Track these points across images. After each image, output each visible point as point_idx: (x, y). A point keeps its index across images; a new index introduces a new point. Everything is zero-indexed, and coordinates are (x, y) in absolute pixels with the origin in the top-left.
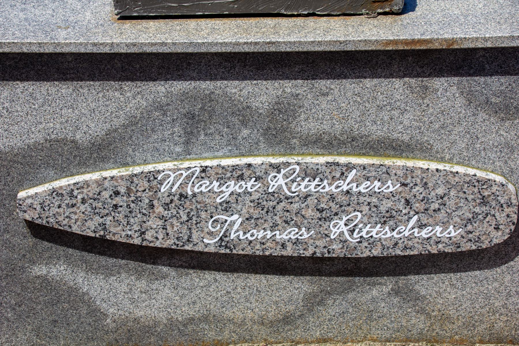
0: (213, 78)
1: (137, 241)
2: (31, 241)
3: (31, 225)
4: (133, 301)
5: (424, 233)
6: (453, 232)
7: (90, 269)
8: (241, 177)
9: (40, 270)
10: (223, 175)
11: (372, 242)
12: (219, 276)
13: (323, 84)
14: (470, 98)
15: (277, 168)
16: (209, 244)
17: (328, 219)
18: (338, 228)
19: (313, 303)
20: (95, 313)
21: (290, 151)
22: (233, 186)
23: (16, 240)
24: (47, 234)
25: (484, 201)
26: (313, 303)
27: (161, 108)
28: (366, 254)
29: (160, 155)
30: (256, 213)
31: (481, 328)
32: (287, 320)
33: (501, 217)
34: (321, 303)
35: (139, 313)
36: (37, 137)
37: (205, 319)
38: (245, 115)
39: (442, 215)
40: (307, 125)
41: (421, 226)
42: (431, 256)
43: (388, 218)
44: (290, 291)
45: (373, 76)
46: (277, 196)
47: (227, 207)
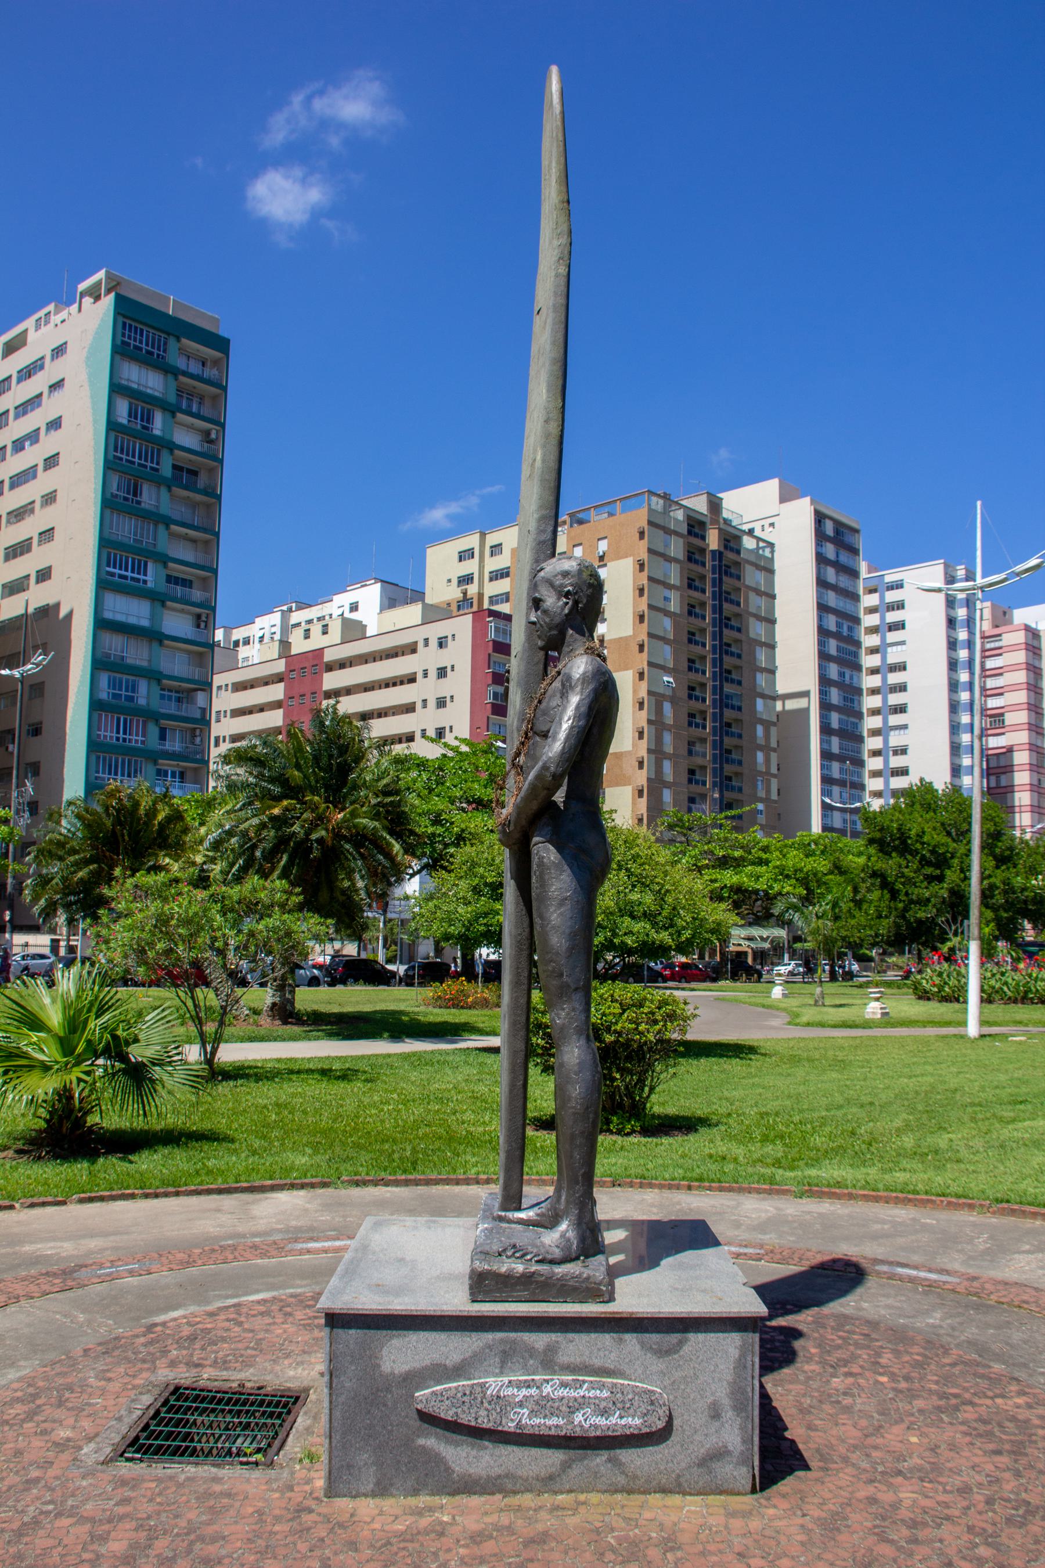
0: (516, 1331)
1: (473, 1424)
2: (419, 1423)
3: (419, 1412)
4: (469, 1463)
5: (623, 1422)
6: (638, 1421)
7: (448, 1442)
8: (529, 1387)
9: (421, 1441)
10: (519, 1385)
11: (596, 1427)
12: (515, 1448)
13: (570, 1335)
14: (642, 1345)
15: (547, 1381)
16: (510, 1426)
17: (573, 1413)
18: (578, 1418)
19: (566, 1466)
20: (448, 1470)
21: (554, 1373)
22: (524, 1392)
23: (412, 1422)
24: (428, 1418)
25: (652, 1403)
26: (566, 1466)
27: (490, 1347)
28: (593, 1434)
29: (488, 1374)
30: (536, 1408)
31: (654, 1483)
32: (551, 1478)
33: (661, 1412)
34: (570, 1467)
35: (472, 1471)
36: (427, 1362)
37: (507, 1476)
38: (531, 1351)
39: (631, 1411)
40: (563, 1358)
41: (621, 1417)
42: (627, 1436)
43: (604, 1413)
44: (554, 1457)
45: (596, 1332)
46: (547, 1398)
47: (521, 1404)
